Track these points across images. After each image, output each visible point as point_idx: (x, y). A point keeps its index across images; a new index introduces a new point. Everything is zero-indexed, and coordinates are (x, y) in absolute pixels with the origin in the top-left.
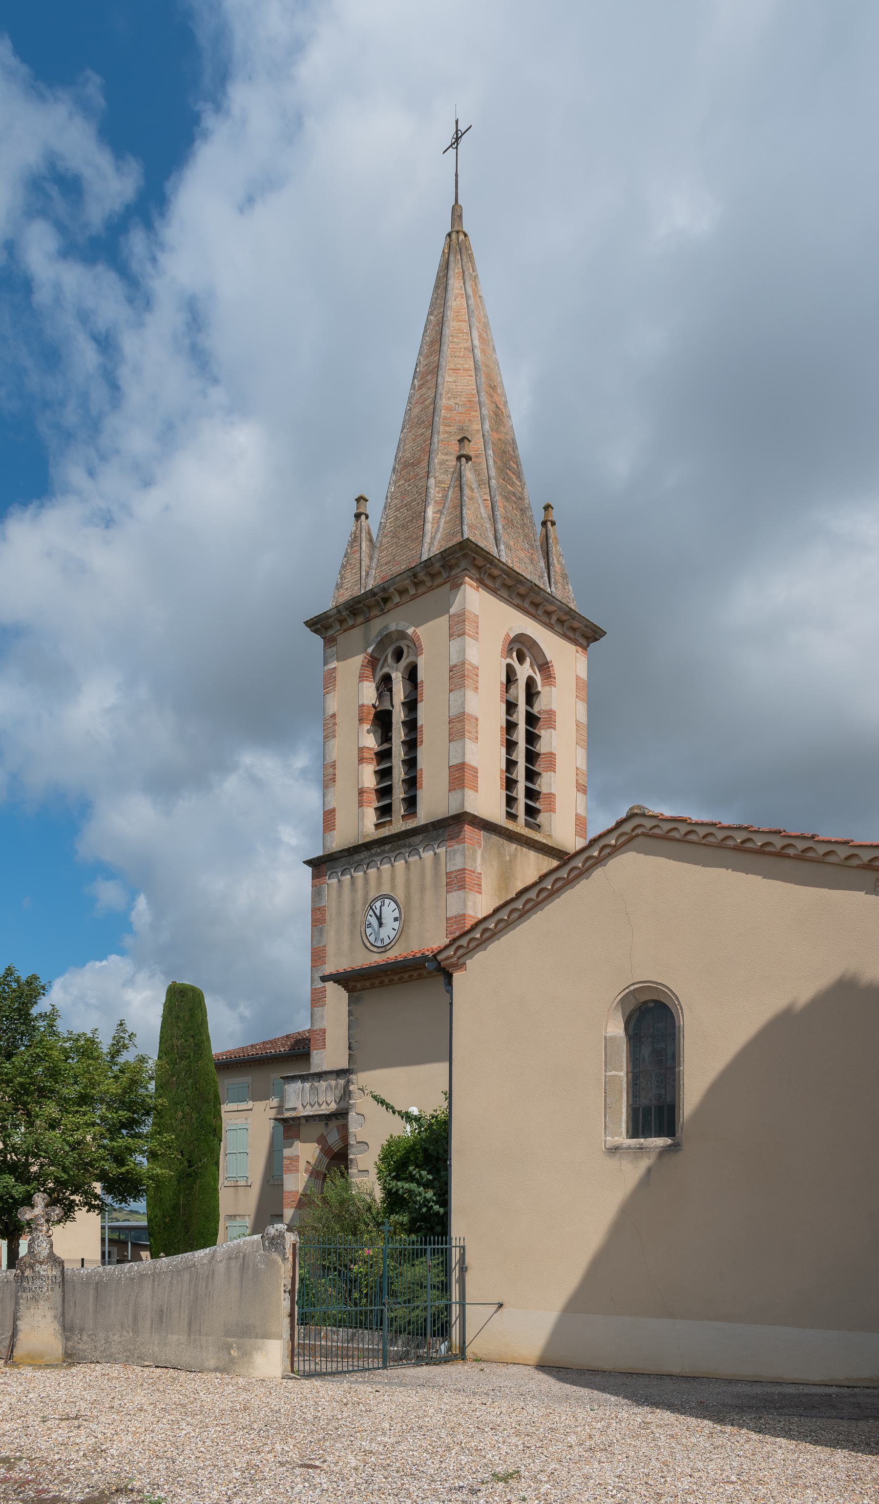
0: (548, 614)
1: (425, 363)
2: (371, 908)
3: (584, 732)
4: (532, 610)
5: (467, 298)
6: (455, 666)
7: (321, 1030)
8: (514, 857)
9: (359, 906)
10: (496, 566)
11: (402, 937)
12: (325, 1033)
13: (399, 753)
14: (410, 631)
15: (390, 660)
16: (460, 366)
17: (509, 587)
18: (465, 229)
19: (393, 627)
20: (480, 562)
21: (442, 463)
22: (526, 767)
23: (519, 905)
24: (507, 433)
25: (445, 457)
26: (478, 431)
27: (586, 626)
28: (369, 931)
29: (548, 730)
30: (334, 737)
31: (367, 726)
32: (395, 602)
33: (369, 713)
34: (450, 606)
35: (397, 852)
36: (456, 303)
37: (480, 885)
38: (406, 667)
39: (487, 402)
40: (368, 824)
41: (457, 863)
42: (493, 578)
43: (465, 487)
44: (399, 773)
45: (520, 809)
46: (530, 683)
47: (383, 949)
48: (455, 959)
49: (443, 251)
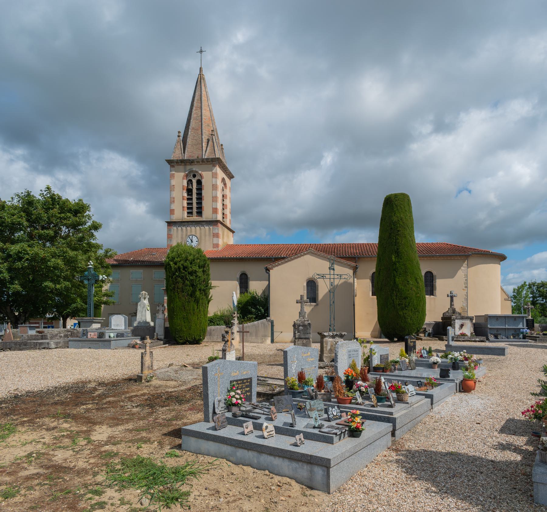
9: (184, 236)
13: (195, 201)
19: (194, 169)
31: (185, 191)
40: (185, 216)
41: (216, 231)
44: (195, 205)
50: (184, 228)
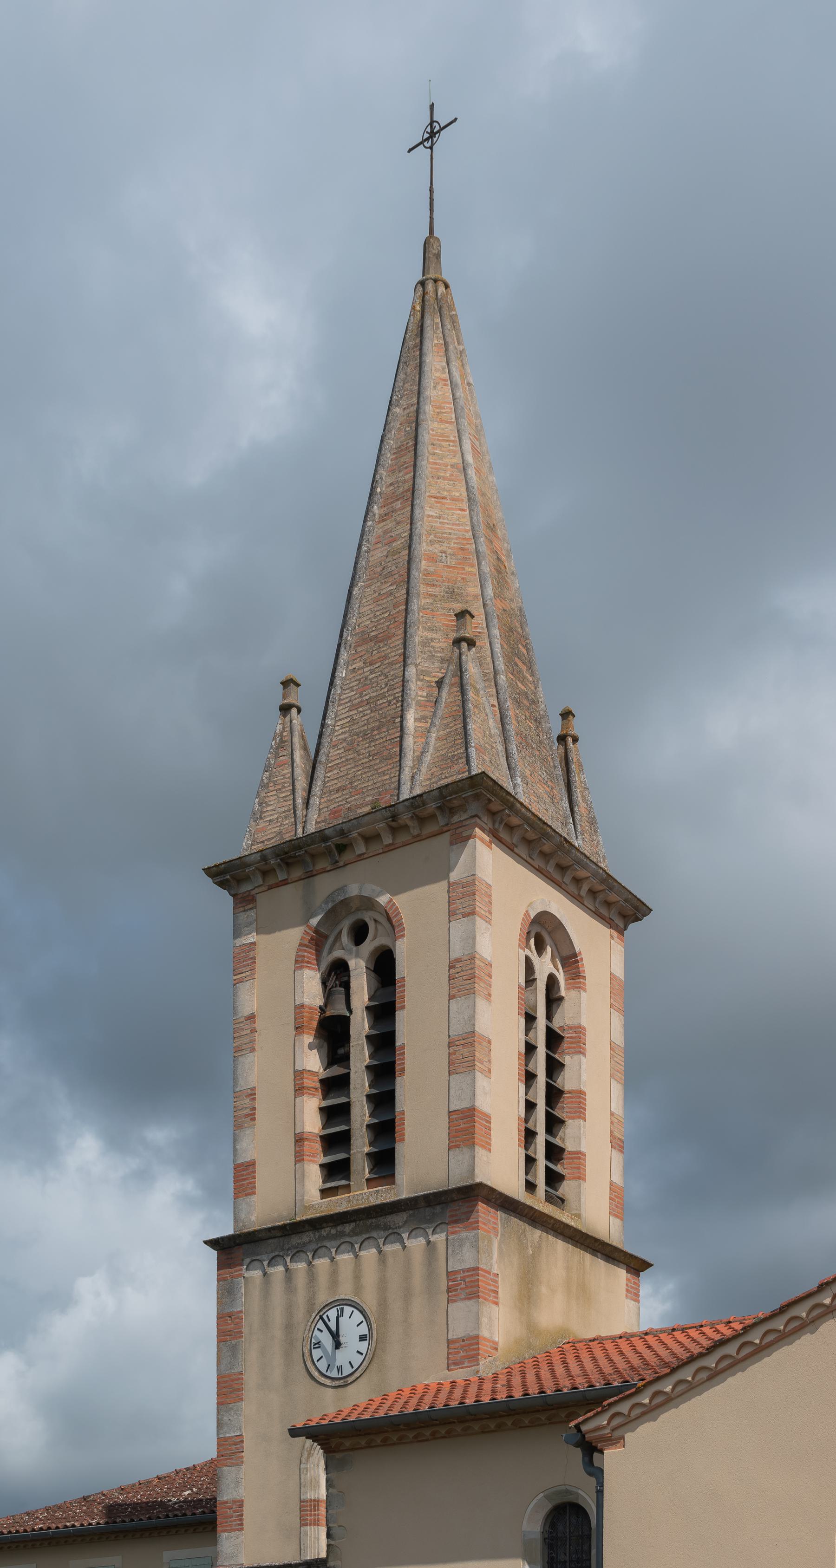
0: (577, 881)
1: (389, 481)
2: (321, 1317)
3: (620, 1059)
4: (557, 876)
5: (453, 387)
6: (458, 960)
7: (235, 1502)
8: (538, 1248)
9: (300, 1313)
10: (517, 813)
11: (374, 1366)
12: (241, 1506)
13: (361, 1085)
14: (383, 900)
15: (345, 939)
16: (445, 493)
17: (528, 842)
18: (445, 276)
19: (353, 890)
20: (496, 806)
21: (425, 643)
22: (547, 1111)
23: (711, 1362)
24: (511, 600)
25: (429, 635)
26: (476, 597)
27: (626, 901)
28: (317, 1354)
29: (576, 1057)
30: (253, 1050)
31: (308, 1038)
32: (358, 852)
33: (311, 1019)
34: (450, 869)
35: (365, 1236)
36: (436, 393)
37: (496, 1292)
38: (373, 953)
39: (487, 552)
40: (310, 1192)
41: (465, 1259)
42: (510, 828)
43: (468, 687)
44: (361, 1115)
45: (540, 1179)
46: (552, 981)
47: (341, 1382)
48: (607, 1431)
49: (413, 308)
50: (300, 1266)
